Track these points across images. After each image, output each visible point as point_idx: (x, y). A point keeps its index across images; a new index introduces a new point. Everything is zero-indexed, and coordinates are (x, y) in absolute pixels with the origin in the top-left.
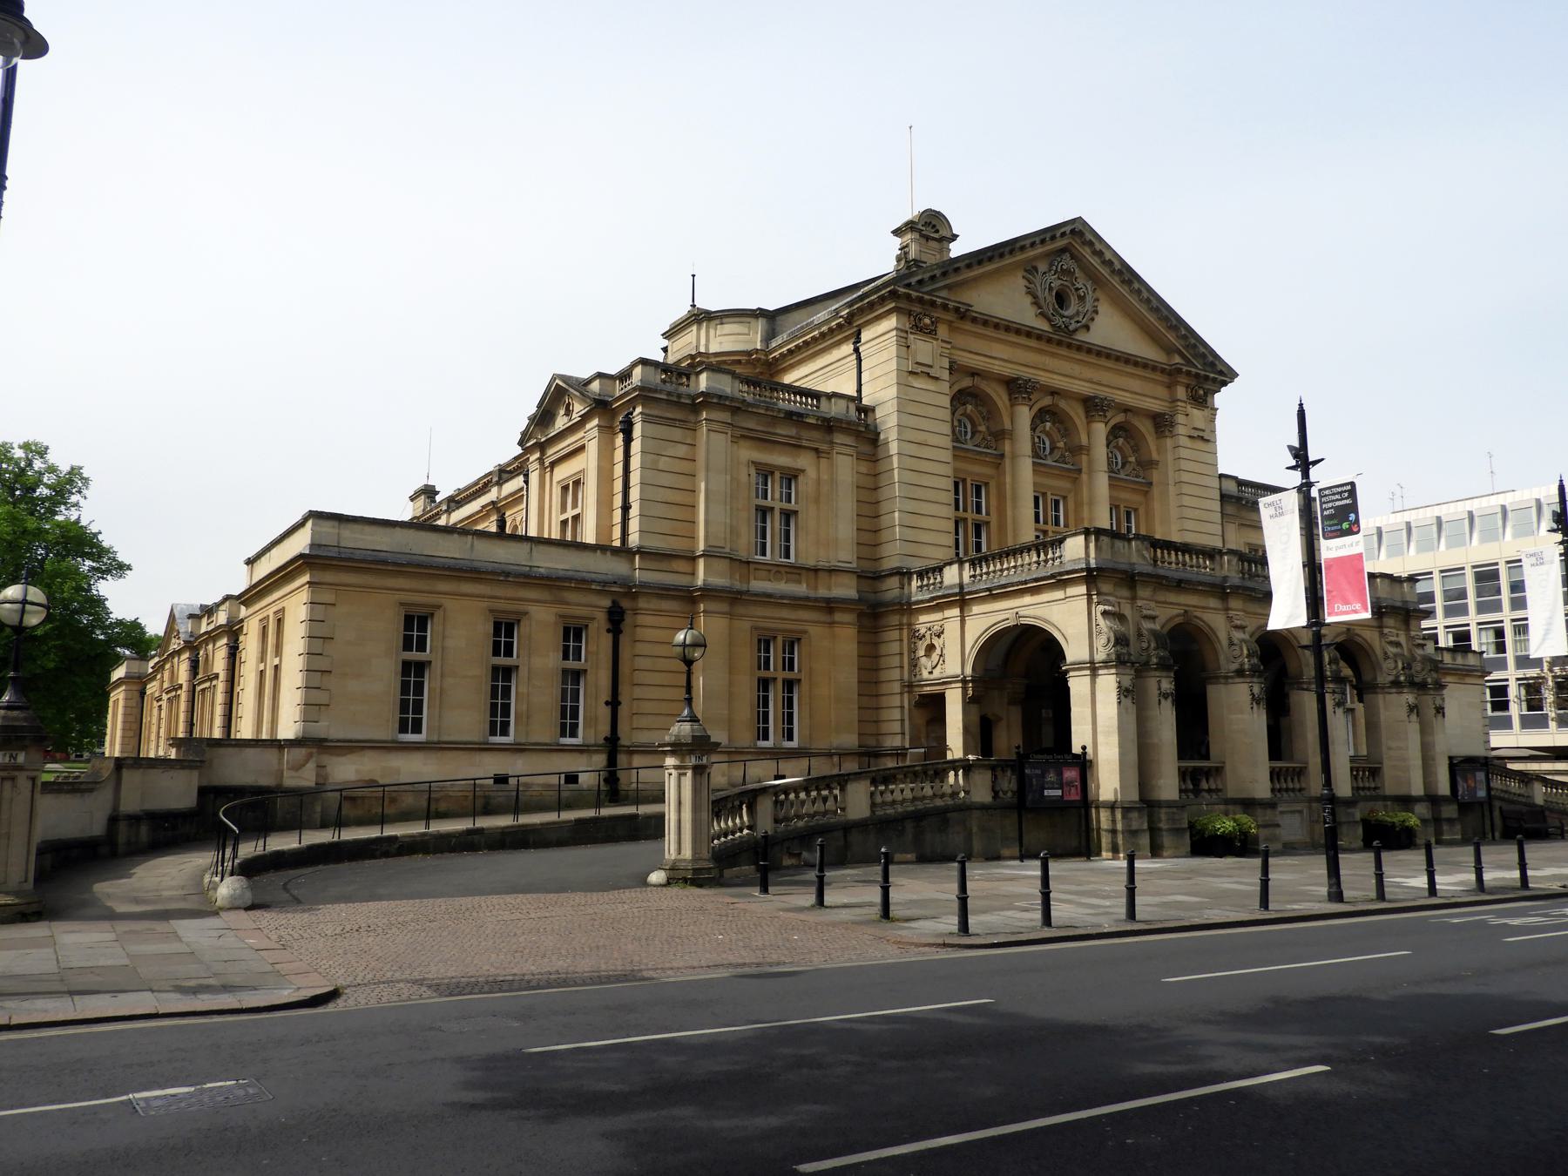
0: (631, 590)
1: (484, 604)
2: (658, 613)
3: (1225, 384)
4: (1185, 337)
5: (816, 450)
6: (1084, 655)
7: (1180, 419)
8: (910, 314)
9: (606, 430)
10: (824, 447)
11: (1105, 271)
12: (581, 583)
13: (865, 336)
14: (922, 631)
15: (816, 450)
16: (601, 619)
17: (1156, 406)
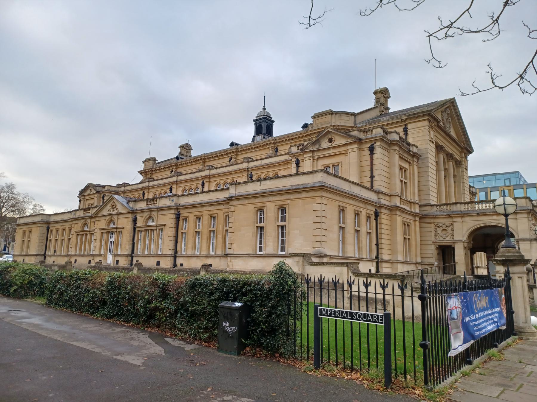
0: (381, 206)
1: (354, 208)
2: (385, 214)
3: (470, 153)
4: (466, 138)
5: (409, 163)
6: (527, 236)
7: (464, 163)
8: (430, 122)
9: (360, 149)
10: (411, 162)
11: (455, 115)
12: (366, 202)
13: (410, 126)
14: (440, 225)
15: (409, 163)
16: (373, 214)
17: (458, 158)
